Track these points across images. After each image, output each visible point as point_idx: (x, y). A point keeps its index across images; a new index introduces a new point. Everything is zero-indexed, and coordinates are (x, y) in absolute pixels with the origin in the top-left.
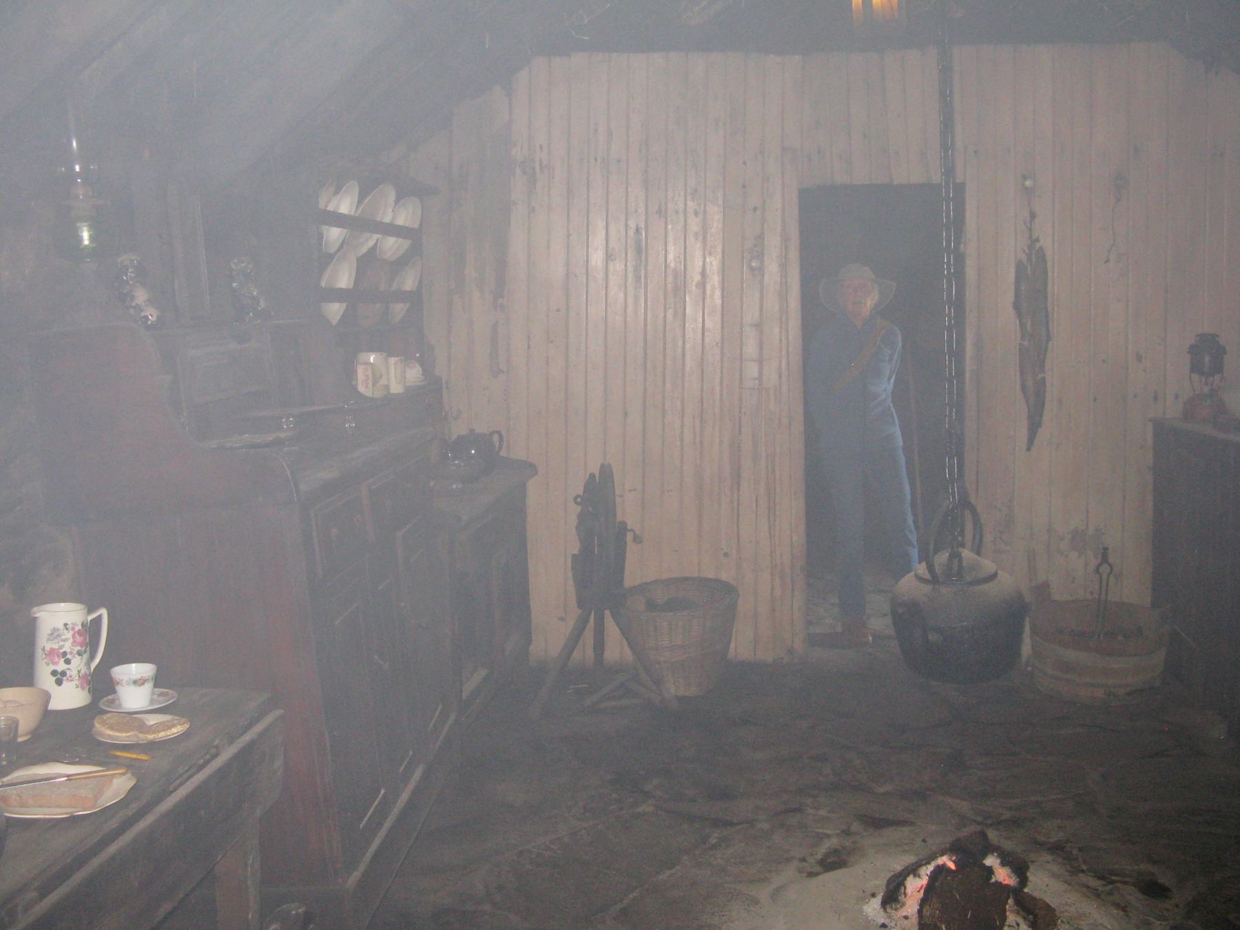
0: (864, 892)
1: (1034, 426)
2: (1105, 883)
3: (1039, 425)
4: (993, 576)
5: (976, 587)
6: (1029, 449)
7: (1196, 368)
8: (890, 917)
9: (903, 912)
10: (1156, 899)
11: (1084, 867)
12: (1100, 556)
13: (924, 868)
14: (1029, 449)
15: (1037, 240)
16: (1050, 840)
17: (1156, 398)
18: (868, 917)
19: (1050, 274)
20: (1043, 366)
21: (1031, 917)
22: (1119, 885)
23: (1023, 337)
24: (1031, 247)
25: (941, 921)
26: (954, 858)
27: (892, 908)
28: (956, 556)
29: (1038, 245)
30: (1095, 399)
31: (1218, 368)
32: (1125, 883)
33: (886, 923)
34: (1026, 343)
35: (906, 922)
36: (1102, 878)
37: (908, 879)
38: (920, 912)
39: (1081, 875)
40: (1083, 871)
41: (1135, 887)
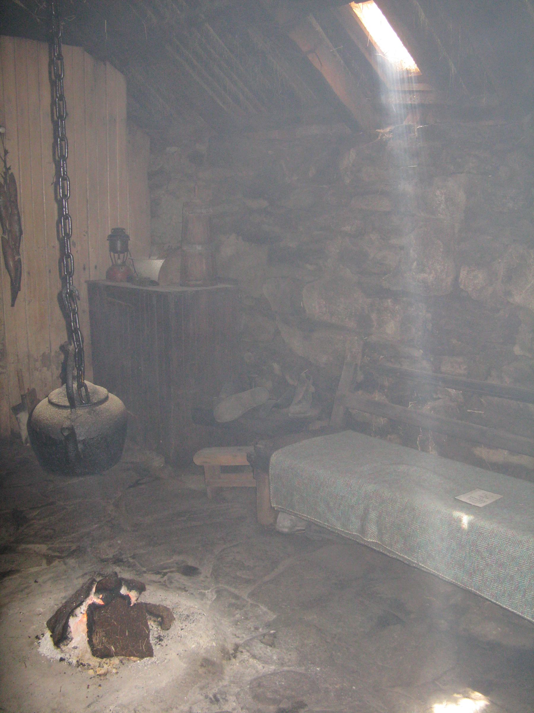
0: (30, 637)
1: (15, 290)
2: (161, 576)
3: (19, 289)
4: (107, 398)
5: (100, 406)
6: (13, 305)
7: (113, 249)
8: (62, 651)
9: (72, 644)
10: (193, 576)
11: (144, 569)
12: (60, 369)
13: (78, 609)
14: (13, 305)
15: (10, 168)
16: (71, 551)
17: (84, 269)
18: (46, 657)
19: (18, 192)
20: (19, 251)
21: (159, 619)
22: (169, 574)
23: (4, 233)
24: (5, 173)
25: (109, 643)
26: (101, 596)
27: (64, 645)
28: (81, 385)
29: (10, 172)
30: (50, 271)
31: (125, 249)
32: (171, 572)
33: (63, 657)
34: (6, 237)
35: (76, 651)
36: (158, 573)
37: (69, 620)
38: (90, 642)
39: (145, 575)
40: (145, 572)
41: (178, 572)
